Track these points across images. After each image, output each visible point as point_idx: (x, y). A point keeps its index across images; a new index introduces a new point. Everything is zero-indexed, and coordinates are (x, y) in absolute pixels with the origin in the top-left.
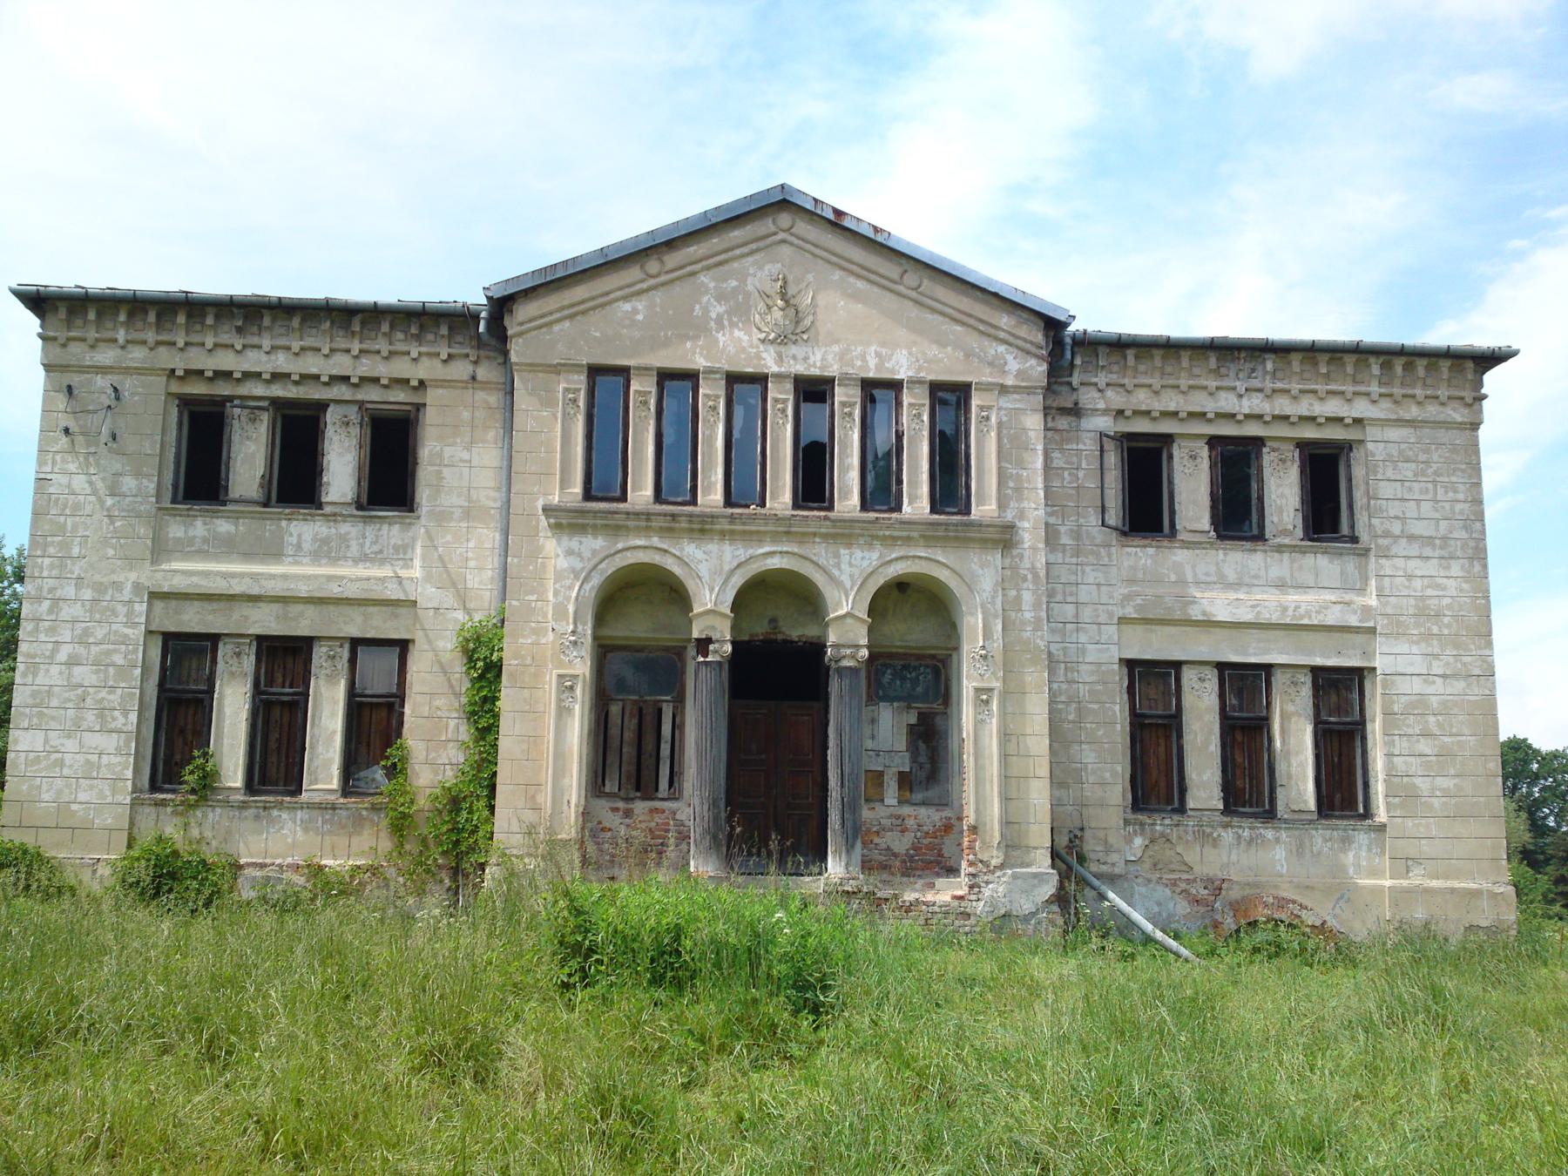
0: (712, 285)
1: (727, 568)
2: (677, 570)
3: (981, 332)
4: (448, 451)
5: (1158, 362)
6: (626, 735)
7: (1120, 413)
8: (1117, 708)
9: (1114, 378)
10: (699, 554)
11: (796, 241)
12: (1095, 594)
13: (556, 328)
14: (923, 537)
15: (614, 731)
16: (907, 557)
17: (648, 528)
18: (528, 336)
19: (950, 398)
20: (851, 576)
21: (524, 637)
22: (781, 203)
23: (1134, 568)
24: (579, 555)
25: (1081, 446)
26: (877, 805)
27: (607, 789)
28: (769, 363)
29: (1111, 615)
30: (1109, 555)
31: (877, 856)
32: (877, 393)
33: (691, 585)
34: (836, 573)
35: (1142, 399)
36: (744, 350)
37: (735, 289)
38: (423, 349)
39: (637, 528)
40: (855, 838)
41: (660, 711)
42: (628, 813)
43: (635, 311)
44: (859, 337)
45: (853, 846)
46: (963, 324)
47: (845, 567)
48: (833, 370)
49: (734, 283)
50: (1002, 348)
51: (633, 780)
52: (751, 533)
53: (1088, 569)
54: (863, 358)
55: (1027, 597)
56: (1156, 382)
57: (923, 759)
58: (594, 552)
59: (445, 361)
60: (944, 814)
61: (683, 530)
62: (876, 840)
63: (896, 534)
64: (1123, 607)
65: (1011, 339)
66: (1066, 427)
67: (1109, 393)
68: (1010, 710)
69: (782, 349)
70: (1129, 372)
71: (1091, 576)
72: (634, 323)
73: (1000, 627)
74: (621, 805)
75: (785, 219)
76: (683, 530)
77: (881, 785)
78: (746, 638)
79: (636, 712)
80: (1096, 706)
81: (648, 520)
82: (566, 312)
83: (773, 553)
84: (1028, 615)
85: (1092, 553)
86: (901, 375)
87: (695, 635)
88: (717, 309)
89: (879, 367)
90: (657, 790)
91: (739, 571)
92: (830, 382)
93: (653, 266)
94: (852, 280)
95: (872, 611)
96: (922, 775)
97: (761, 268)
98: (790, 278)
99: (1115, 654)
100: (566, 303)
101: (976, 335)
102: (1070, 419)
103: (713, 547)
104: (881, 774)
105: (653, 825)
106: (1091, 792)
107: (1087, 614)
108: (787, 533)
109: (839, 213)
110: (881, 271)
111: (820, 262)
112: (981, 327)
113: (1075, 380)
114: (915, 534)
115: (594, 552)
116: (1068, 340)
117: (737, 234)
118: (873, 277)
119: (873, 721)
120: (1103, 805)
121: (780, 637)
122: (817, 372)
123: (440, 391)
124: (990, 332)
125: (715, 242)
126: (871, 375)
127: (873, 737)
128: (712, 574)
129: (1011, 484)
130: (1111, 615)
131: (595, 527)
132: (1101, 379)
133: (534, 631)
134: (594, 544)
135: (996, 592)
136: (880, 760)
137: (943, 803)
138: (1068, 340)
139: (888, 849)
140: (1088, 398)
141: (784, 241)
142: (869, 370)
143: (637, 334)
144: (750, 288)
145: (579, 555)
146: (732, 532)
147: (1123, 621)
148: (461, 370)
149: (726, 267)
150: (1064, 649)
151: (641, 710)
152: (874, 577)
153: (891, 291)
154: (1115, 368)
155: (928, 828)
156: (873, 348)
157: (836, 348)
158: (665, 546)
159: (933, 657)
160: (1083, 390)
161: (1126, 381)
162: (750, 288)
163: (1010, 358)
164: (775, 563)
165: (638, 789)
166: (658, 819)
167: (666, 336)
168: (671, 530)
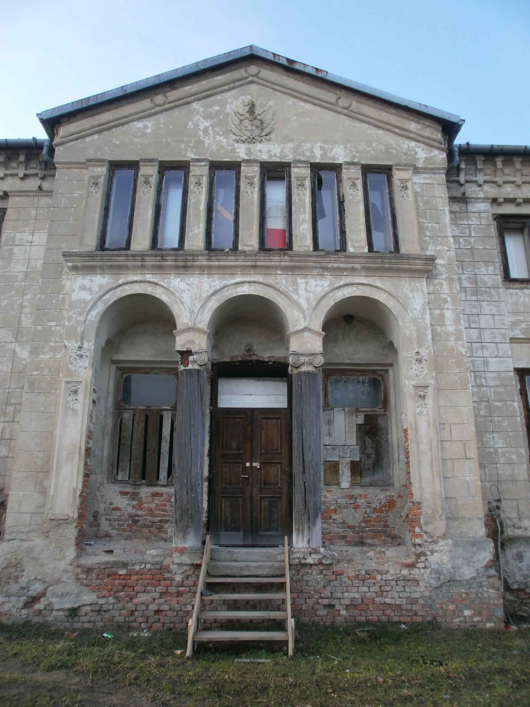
0: (201, 110)
1: (205, 295)
2: (164, 298)
3: (397, 134)
4: (18, 236)
5: (518, 166)
6: (135, 435)
7: (494, 201)
8: (516, 404)
9: (488, 178)
10: (183, 286)
11: (261, 82)
12: (491, 321)
13: (88, 139)
14: (365, 268)
15: (127, 434)
16: (352, 284)
17: (143, 267)
18: (68, 145)
19: (377, 174)
20: (308, 299)
21: (43, 353)
22: (252, 58)
23: (516, 304)
24: (90, 290)
25: (470, 222)
26: (334, 488)
27: (120, 477)
28: (241, 152)
29: (504, 336)
30: (498, 294)
31: (335, 529)
32: (324, 175)
33: (176, 310)
34: (295, 297)
35: (509, 191)
36: (223, 148)
37: (219, 111)
38: (8, 172)
39: (135, 268)
40: (316, 516)
41: (162, 417)
42: (134, 496)
43: (146, 127)
44: (307, 133)
45: (314, 523)
46: (383, 129)
47: (302, 292)
48: (289, 158)
49: (217, 108)
50: (413, 144)
51: (140, 470)
52: (225, 267)
53: (484, 304)
54: (311, 150)
55: (449, 315)
56: (519, 179)
57: (369, 451)
58: (101, 286)
59: (22, 179)
60: (388, 493)
61: (171, 267)
62: (334, 516)
63: (342, 266)
64: (513, 330)
65: (419, 138)
66: (458, 210)
67: (486, 187)
68: (442, 403)
69: (251, 146)
70: (499, 173)
71: (487, 309)
72: (144, 135)
73: (430, 337)
74: (129, 489)
75: (253, 69)
76: (171, 267)
77: (337, 472)
78: (227, 359)
79: (143, 418)
80: (500, 404)
81: (143, 260)
82: (97, 129)
83: (243, 282)
84: (451, 329)
85: (486, 293)
86: (340, 161)
87: (178, 348)
88: (204, 124)
89: (324, 156)
90: (158, 479)
91: (214, 298)
92: (288, 165)
93: (159, 99)
94: (301, 104)
95: (324, 329)
96: (370, 462)
97: (236, 98)
98: (257, 104)
99: (511, 365)
100: (96, 123)
101: (392, 135)
102: (460, 205)
103: (195, 280)
104: (336, 465)
105: (153, 506)
106: (504, 471)
107: (487, 336)
108: (254, 267)
109: (290, 61)
110: (323, 97)
111: (279, 94)
112: (396, 130)
113: (462, 178)
114: (358, 266)
115: (101, 286)
116: (456, 149)
117: (220, 79)
118: (316, 101)
119: (330, 422)
120: (513, 480)
121: (254, 358)
122: (278, 160)
123: (18, 199)
124: (406, 134)
125: (204, 84)
126: (318, 161)
127: (330, 435)
128: (193, 301)
129: (428, 234)
130: (504, 336)
131: (102, 268)
132: (480, 178)
133: (52, 349)
134: (100, 281)
135: (425, 310)
136: (336, 452)
137: (387, 484)
138: (456, 149)
139: (344, 523)
140: (471, 190)
141: (252, 82)
142: (316, 158)
143: (146, 141)
144: (228, 110)
145: (90, 290)
146: (210, 267)
147: (514, 340)
148: (32, 184)
149: (212, 99)
150: (473, 362)
151: (147, 416)
152: (326, 300)
153: (330, 110)
154: (489, 172)
155: (376, 505)
156: (318, 145)
157: (291, 145)
158: (156, 280)
159: (374, 372)
160: (467, 185)
161: (497, 179)
162: (228, 110)
163: (419, 150)
164: (245, 290)
165: (144, 478)
166: (157, 501)
167: (167, 142)
168: (160, 268)
